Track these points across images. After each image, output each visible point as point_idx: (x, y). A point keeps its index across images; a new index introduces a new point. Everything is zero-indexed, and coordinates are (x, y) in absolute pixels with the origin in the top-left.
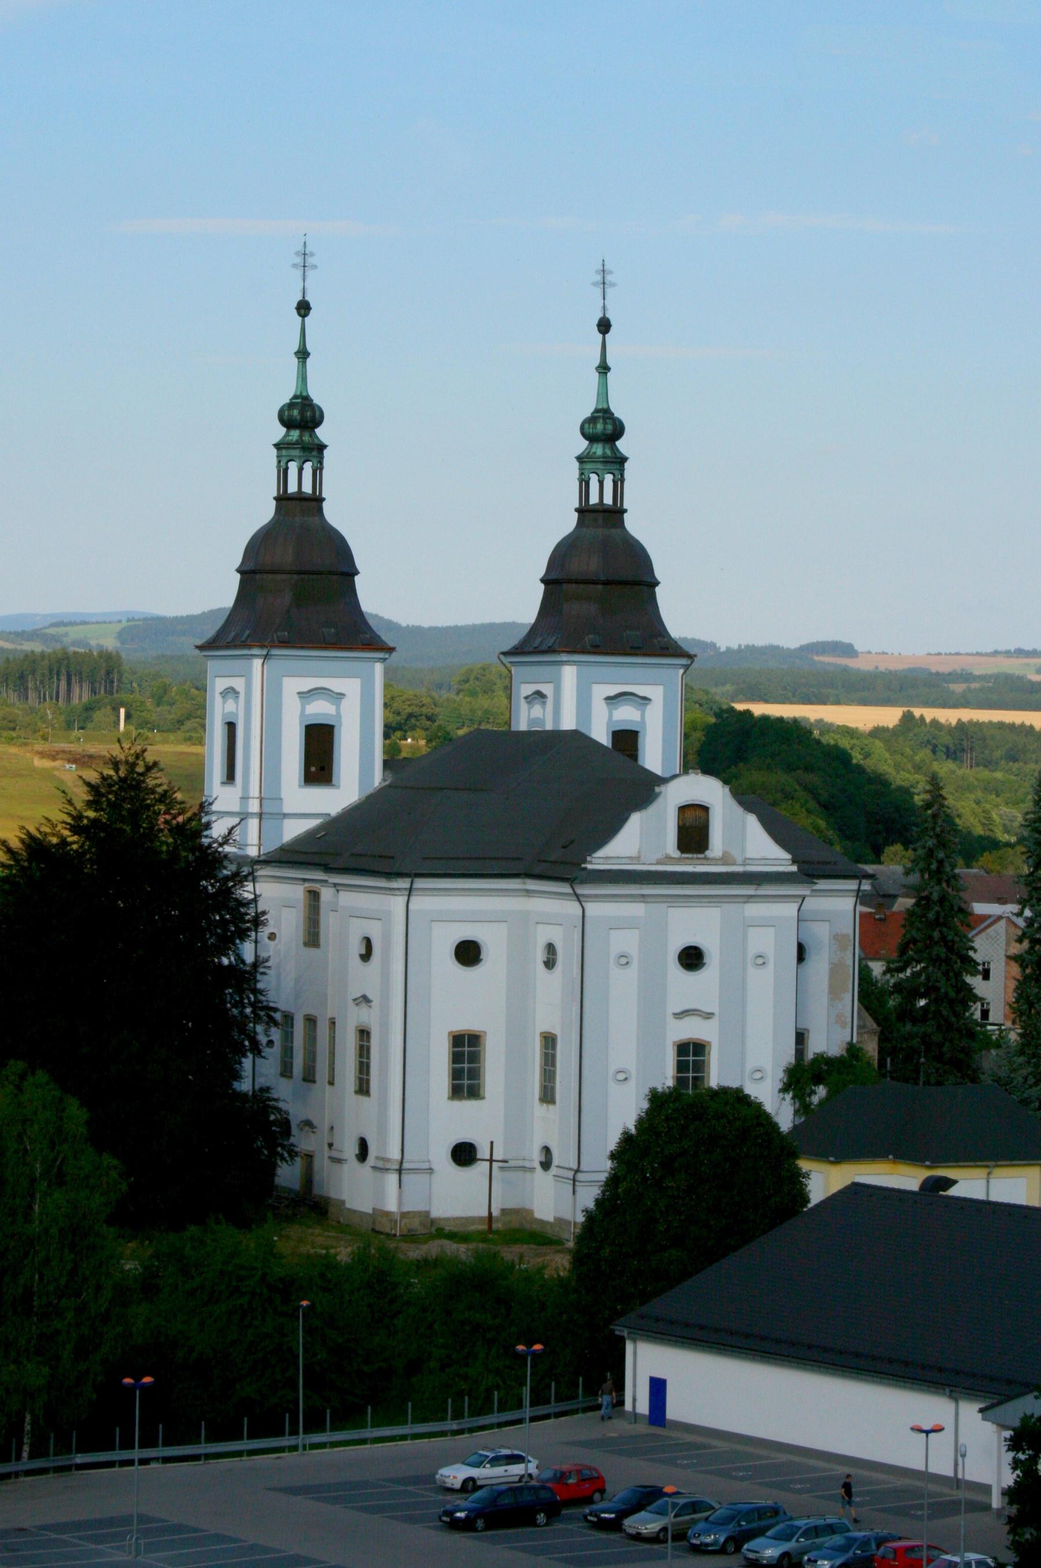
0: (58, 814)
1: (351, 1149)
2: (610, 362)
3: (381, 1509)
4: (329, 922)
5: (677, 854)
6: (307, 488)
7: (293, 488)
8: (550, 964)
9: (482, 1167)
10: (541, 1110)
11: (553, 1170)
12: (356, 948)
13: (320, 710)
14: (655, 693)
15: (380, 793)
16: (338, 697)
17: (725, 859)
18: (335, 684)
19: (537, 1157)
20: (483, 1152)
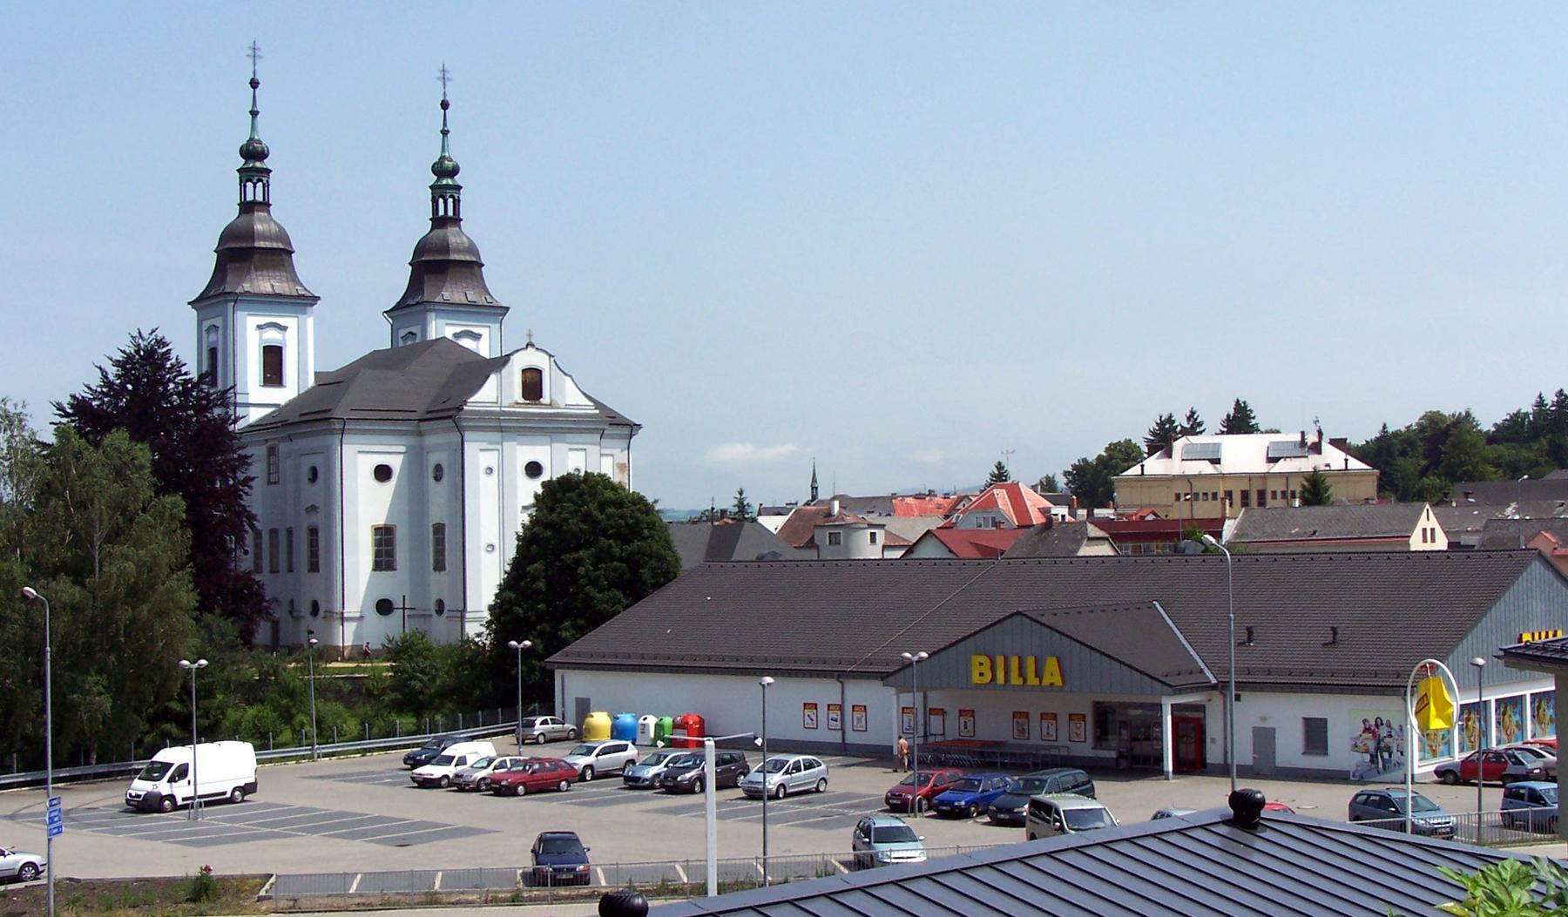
0: (96, 381)
1: (306, 609)
2: (448, 127)
3: (363, 835)
4: (286, 465)
5: (522, 400)
6: (260, 198)
7: (250, 198)
8: (438, 478)
9: (397, 614)
10: (435, 577)
11: (446, 614)
12: (305, 474)
13: (273, 336)
14: (484, 331)
15: (309, 392)
16: (284, 329)
17: (550, 405)
18: (282, 321)
19: (433, 608)
20: (398, 603)
